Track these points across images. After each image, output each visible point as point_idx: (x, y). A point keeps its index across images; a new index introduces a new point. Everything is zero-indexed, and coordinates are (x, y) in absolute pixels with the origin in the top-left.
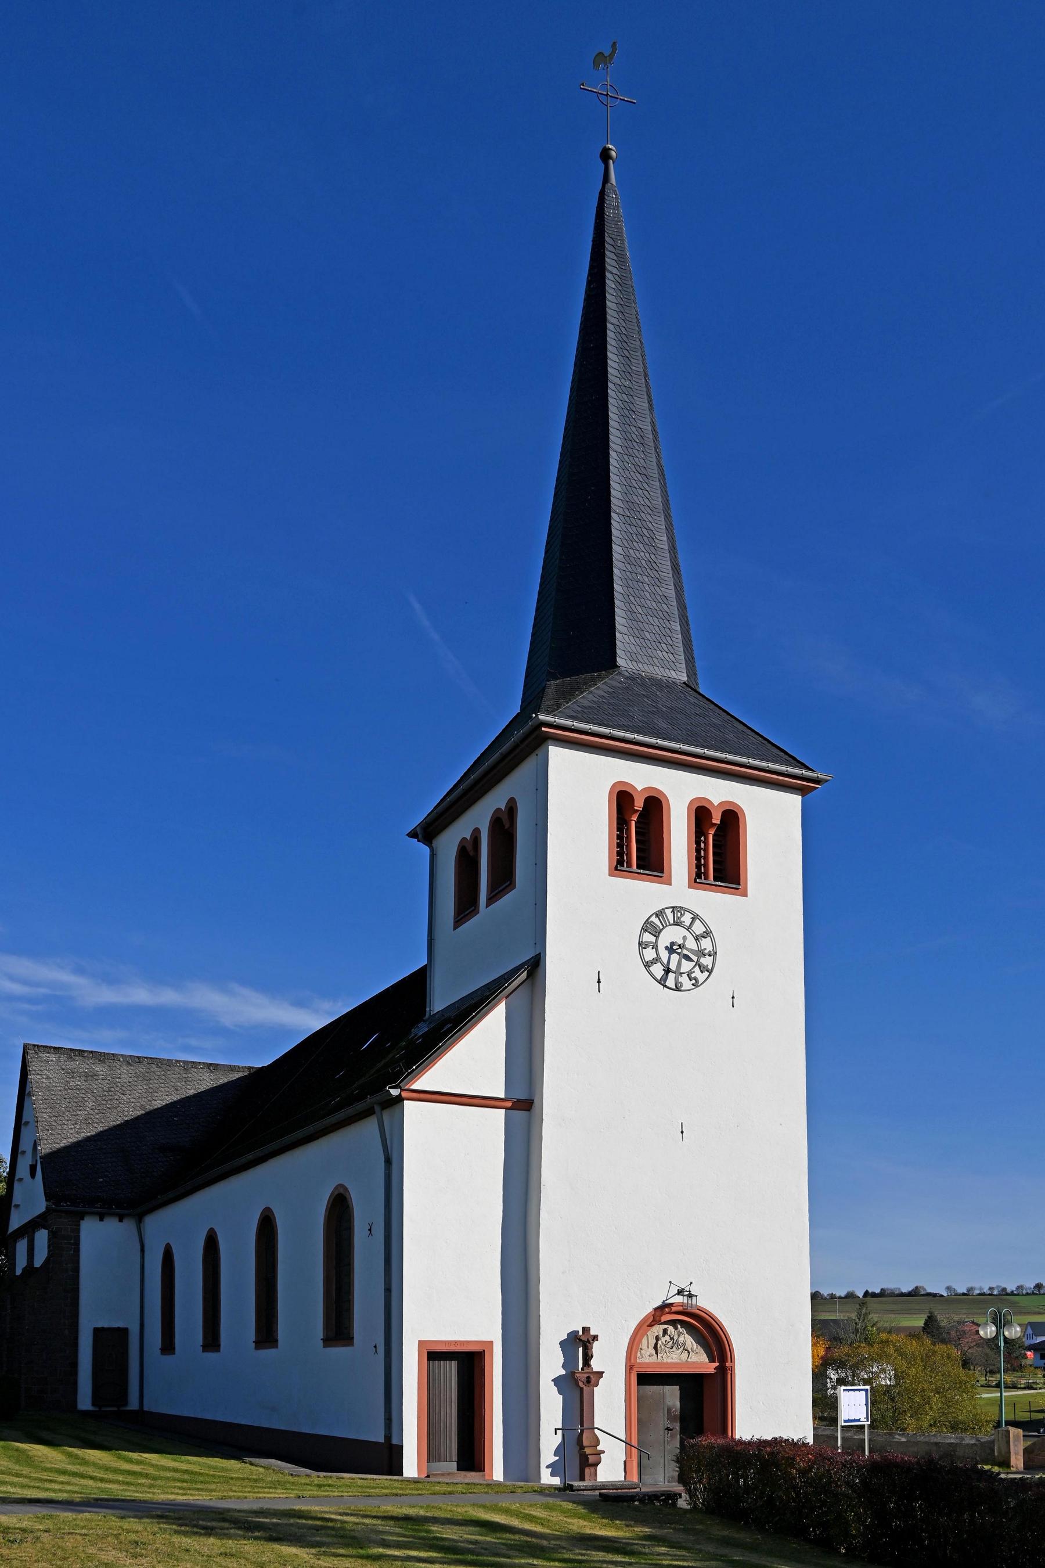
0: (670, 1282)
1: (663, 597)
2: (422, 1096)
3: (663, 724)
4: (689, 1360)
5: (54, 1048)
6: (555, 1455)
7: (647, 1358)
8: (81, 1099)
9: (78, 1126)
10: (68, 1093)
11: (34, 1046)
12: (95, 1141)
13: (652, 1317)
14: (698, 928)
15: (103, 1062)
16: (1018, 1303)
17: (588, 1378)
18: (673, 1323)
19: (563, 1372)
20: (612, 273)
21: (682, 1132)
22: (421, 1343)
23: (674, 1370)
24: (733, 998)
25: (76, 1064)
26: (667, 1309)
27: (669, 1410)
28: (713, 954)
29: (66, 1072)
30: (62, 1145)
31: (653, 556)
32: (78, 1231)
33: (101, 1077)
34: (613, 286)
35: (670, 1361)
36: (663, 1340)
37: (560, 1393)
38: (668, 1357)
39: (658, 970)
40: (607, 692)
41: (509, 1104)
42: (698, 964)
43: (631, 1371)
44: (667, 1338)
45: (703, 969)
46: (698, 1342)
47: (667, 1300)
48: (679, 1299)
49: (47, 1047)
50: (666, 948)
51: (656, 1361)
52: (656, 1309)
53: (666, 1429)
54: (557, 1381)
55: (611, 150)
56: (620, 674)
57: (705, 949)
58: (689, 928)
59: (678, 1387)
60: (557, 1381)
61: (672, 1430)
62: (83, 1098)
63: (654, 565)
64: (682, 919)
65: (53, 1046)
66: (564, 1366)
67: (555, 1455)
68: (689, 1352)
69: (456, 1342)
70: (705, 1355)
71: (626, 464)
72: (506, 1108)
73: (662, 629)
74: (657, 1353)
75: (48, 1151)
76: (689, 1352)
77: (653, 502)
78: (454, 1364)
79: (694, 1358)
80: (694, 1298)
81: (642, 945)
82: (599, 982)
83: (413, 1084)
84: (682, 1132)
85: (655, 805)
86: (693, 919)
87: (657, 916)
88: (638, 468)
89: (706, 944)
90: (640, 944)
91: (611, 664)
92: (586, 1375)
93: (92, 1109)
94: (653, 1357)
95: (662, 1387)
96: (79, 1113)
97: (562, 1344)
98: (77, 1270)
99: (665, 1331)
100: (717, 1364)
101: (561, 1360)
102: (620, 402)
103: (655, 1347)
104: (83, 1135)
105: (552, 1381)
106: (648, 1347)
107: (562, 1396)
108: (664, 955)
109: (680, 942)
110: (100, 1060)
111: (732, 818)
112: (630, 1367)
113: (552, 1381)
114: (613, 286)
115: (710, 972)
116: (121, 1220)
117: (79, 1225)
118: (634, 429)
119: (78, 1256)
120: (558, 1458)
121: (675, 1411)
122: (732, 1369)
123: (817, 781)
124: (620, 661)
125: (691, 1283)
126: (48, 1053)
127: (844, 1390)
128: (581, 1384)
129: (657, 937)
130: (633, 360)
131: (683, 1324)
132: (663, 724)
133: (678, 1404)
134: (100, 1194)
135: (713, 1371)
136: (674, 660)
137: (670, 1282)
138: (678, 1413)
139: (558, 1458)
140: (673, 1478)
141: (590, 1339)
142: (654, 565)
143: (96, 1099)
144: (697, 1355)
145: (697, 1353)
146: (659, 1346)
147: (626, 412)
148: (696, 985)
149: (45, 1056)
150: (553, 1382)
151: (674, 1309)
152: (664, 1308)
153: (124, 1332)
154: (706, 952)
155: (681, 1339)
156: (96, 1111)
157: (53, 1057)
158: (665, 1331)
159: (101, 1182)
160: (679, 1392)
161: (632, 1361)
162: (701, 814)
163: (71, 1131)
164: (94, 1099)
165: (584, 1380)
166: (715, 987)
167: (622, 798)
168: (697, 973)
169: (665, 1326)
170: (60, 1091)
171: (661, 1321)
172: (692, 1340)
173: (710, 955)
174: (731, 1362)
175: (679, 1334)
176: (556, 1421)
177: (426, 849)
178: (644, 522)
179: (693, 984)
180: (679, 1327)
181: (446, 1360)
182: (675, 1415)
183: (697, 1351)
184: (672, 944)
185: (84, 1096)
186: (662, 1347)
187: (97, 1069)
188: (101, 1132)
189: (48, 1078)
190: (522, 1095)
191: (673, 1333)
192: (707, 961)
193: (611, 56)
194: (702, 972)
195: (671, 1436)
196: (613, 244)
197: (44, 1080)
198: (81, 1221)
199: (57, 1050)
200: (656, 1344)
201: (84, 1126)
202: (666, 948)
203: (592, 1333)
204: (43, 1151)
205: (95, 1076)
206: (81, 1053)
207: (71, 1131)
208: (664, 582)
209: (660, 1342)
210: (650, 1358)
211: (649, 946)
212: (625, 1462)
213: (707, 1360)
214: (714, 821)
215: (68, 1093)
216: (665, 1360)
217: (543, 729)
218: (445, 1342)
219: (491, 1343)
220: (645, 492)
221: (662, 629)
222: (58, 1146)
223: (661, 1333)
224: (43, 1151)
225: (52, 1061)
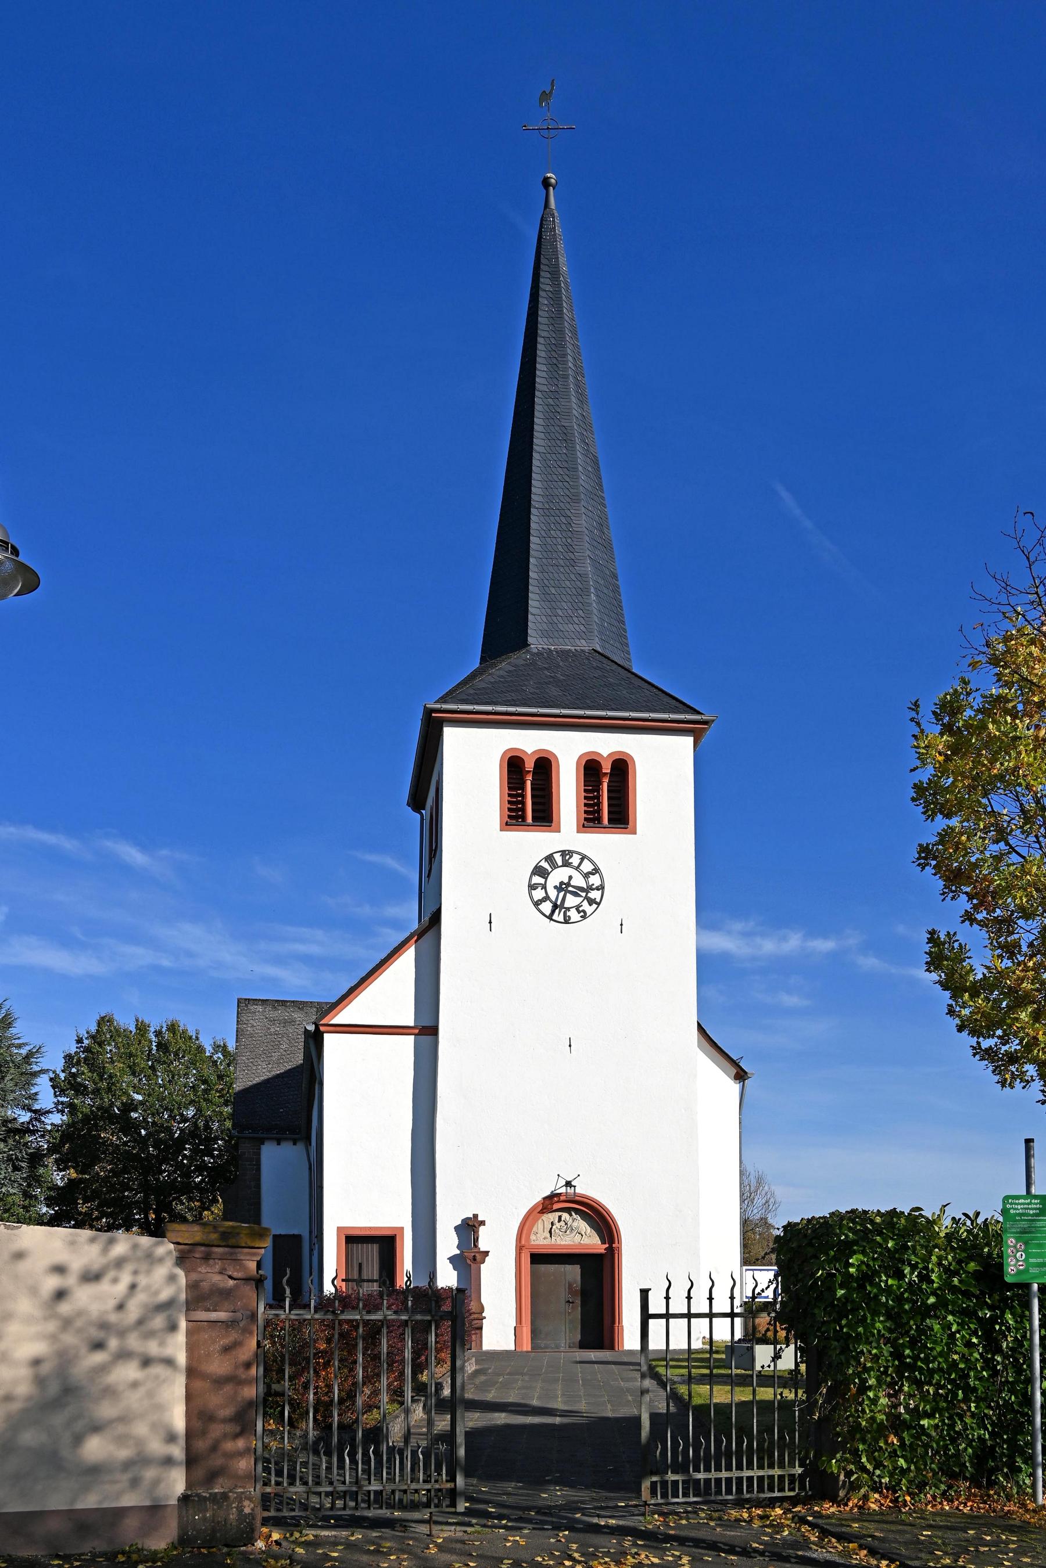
0: (558, 1175)
1: (577, 576)
2: (338, 1029)
3: (554, 691)
4: (582, 1242)
5: (263, 1000)
7: (541, 1239)
8: (277, 1043)
9: (270, 1066)
10: (267, 1038)
11: (246, 999)
12: (283, 1078)
14: (587, 867)
15: (301, 1009)
17: (474, 1257)
18: (568, 1210)
19: (458, 1252)
20: (546, 291)
21: (570, 1046)
22: (340, 1229)
23: (565, 1251)
24: (621, 925)
25: (280, 1013)
27: (570, 1285)
28: (601, 888)
29: (269, 1021)
30: (254, 1082)
31: (569, 540)
32: (259, 1154)
33: (298, 1022)
34: (546, 302)
35: (563, 1243)
36: (558, 1225)
39: (547, 907)
40: (509, 672)
41: (417, 1031)
42: (587, 898)
44: (562, 1223)
45: (591, 902)
46: (592, 1227)
48: (563, 1190)
49: (256, 1000)
50: (555, 887)
52: (544, 1199)
54: (452, 1260)
55: (550, 178)
56: (528, 652)
57: (593, 885)
58: (577, 868)
59: (579, 1266)
60: (452, 1260)
61: (573, 1303)
62: (279, 1041)
63: (570, 548)
64: (570, 861)
65: (261, 998)
66: (458, 1247)
68: (582, 1236)
69: (370, 1228)
70: (598, 1238)
71: (548, 462)
72: (415, 1035)
73: (574, 604)
74: (551, 1237)
75: (241, 1088)
76: (582, 1236)
77: (572, 490)
78: (376, 1247)
79: (586, 1241)
80: (573, 1188)
81: (532, 887)
82: (490, 922)
83: (333, 1018)
84: (570, 1046)
85: (545, 765)
86: (582, 860)
87: (546, 860)
88: (559, 463)
89: (595, 880)
90: (529, 886)
91: (524, 644)
92: (473, 1254)
93: (285, 1051)
95: (563, 1266)
96: (273, 1054)
97: (457, 1229)
98: (258, 1186)
99: (560, 1217)
100: (607, 1245)
101: (456, 1242)
102: (546, 407)
104: (273, 1073)
108: (553, 894)
109: (566, 881)
110: (299, 1008)
111: (622, 767)
112: (520, 1249)
114: (546, 302)
115: (599, 904)
116: (295, 1144)
117: (260, 1149)
118: (557, 428)
119: (259, 1175)
121: (576, 1287)
122: (619, 1249)
123: (706, 723)
124: (530, 640)
125: (579, 1175)
126: (257, 1005)
127: (747, 1270)
128: (469, 1262)
129: (546, 879)
130: (560, 366)
131: (577, 1211)
132: (554, 691)
133: (579, 1278)
134: (278, 1123)
135: (603, 1251)
136: (584, 630)
137: (558, 1175)
138: (579, 1288)
140: (573, 1343)
141: (477, 1225)
142: (570, 548)
143: (290, 1042)
145: (590, 1236)
146: (553, 1230)
147: (551, 414)
148: (584, 917)
149: (252, 1008)
151: (562, 1198)
152: (552, 1197)
153: (297, 1238)
154: (594, 887)
155: (575, 1224)
156: (288, 1052)
157: (260, 1008)
158: (560, 1217)
159: (281, 1112)
161: (523, 1242)
162: (590, 768)
163: (264, 1071)
164: (288, 1042)
165: (471, 1258)
166: (602, 918)
167: (514, 765)
168: (585, 906)
169: (560, 1214)
170: (261, 1037)
173: (598, 890)
175: (574, 1220)
177: (418, 816)
178: (562, 511)
179: (581, 917)
180: (573, 1214)
181: (367, 1243)
182: (576, 1290)
184: (562, 883)
185: (280, 1040)
187: (296, 1016)
188: (290, 1070)
189: (253, 1026)
190: (427, 1022)
191: (568, 1219)
192: (595, 895)
193: (551, 92)
194: (590, 905)
195: (572, 1308)
196: (549, 264)
197: (249, 1029)
198: (262, 1146)
199: (264, 1002)
200: (551, 1228)
201: (276, 1065)
202: (555, 887)
203: (480, 1219)
204: (238, 1089)
205: (292, 1022)
206: (283, 1003)
207: (264, 1071)
208: (579, 561)
209: (554, 1227)
211: (537, 888)
214: (604, 771)
215: (267, 1038)
216: (559, 1242)
217: (433, 715)
218: (361, 1228)
219: (402, 1228)
220: (565, 483)
221: (574, 604)
222: (250, 1084)
224: (238, 1088)
225: (259, 1011)
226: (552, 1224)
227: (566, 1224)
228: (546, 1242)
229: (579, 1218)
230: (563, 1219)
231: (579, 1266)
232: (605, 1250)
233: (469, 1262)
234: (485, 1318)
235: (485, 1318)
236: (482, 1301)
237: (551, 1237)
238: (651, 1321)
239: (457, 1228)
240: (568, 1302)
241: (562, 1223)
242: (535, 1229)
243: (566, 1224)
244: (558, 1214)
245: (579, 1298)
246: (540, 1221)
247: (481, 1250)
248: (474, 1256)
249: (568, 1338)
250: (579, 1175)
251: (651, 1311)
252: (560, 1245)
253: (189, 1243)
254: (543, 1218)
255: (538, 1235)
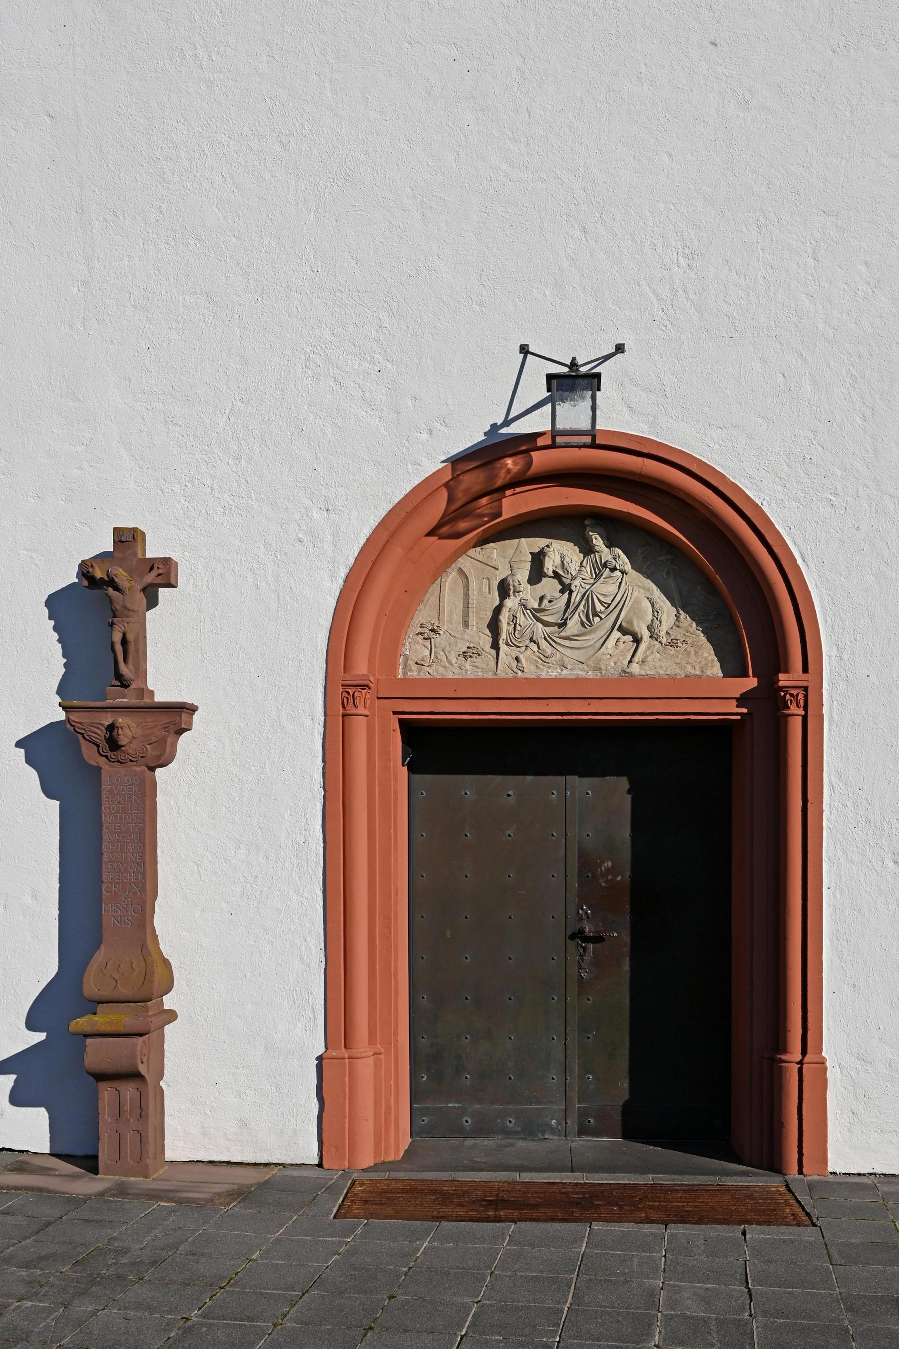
0: (524, 350)
4: (635, 669)
6: (31, 1024)
13: (444, 494)
16: (56, 1170)
26: (509, 461)
37: (49, 791)
38: (545, 658)
43: (351, 710)
44: (549, 586)
46: (681, 602)
47: (507, 423)
51: (490, 675)
52: (456, 461)
53: (573, 937)
59: (623, 783)
61: (597, 939)
67: (31, 1024)
68: (637, 640)
74: (495, 646)
92: (107, 719)
94: (478, 660)
95: (560, 779)
99: (538, 558)
100: (751, 682)
103: (494, 626)
105: (19, 744)
106: (466, 624)
107: (57, 803)
113: (19, 744)
120: (41, 1036)
125: (620, 348)
137: (524, 350)
138: (623, 877)
139: (41, 1036)
144: (672, 651)
145: (673, 643)
146: (504, 618)
150: (22, 752)
151: (540, 460)
158: (538, 558)
160: (629, 798)
161: (361, 668)
165: (100, 735)
171: (499, 514)
172: (657, 593)
174: (805, 670)
176: (34, 897)
180: (598, 542)
183: (677, 634)
186: (521, 619)
191: (573, 568)
200: (498, 611)
209: (511, 603)
210: (468, 665)
212: (320, 1059)
213: (716, 670)
216: (530, 670)
223: (523, 574)
226: (504, 589)
227: (566, 588)
228: (470, 670)
229: (624, 561)
230: (549, 566)
231: (623, 783)
232: (742, 700)
233: (90, 754)
234: (172, 1016)
235: (172, 1016)
236: (50, 967)
237: (495, 646)
238: (598, 442)
239: (53, 602)
240: (579, 935)
241: (549, 586)
242: (423, 615)
243: (566, 588)
244: (529, 545)
245: (626, 919)
246: (450, 579)
247: (159, 698)
248: (111, 728)
249: (574, 1094)
250: (620, 348)
251: (550, 443)
252: (538, 681)
253: (77, 721)
254: (464, 562)
255: (437, 640)
